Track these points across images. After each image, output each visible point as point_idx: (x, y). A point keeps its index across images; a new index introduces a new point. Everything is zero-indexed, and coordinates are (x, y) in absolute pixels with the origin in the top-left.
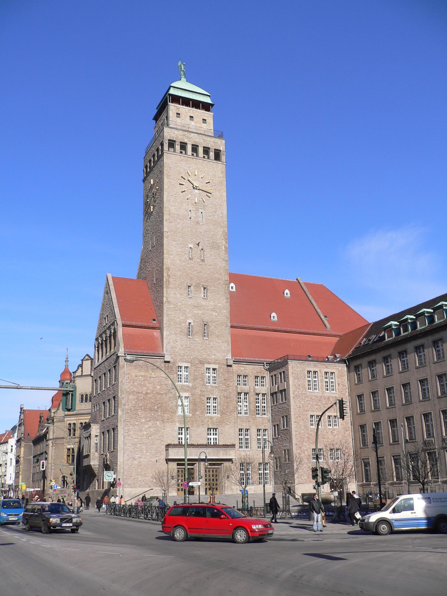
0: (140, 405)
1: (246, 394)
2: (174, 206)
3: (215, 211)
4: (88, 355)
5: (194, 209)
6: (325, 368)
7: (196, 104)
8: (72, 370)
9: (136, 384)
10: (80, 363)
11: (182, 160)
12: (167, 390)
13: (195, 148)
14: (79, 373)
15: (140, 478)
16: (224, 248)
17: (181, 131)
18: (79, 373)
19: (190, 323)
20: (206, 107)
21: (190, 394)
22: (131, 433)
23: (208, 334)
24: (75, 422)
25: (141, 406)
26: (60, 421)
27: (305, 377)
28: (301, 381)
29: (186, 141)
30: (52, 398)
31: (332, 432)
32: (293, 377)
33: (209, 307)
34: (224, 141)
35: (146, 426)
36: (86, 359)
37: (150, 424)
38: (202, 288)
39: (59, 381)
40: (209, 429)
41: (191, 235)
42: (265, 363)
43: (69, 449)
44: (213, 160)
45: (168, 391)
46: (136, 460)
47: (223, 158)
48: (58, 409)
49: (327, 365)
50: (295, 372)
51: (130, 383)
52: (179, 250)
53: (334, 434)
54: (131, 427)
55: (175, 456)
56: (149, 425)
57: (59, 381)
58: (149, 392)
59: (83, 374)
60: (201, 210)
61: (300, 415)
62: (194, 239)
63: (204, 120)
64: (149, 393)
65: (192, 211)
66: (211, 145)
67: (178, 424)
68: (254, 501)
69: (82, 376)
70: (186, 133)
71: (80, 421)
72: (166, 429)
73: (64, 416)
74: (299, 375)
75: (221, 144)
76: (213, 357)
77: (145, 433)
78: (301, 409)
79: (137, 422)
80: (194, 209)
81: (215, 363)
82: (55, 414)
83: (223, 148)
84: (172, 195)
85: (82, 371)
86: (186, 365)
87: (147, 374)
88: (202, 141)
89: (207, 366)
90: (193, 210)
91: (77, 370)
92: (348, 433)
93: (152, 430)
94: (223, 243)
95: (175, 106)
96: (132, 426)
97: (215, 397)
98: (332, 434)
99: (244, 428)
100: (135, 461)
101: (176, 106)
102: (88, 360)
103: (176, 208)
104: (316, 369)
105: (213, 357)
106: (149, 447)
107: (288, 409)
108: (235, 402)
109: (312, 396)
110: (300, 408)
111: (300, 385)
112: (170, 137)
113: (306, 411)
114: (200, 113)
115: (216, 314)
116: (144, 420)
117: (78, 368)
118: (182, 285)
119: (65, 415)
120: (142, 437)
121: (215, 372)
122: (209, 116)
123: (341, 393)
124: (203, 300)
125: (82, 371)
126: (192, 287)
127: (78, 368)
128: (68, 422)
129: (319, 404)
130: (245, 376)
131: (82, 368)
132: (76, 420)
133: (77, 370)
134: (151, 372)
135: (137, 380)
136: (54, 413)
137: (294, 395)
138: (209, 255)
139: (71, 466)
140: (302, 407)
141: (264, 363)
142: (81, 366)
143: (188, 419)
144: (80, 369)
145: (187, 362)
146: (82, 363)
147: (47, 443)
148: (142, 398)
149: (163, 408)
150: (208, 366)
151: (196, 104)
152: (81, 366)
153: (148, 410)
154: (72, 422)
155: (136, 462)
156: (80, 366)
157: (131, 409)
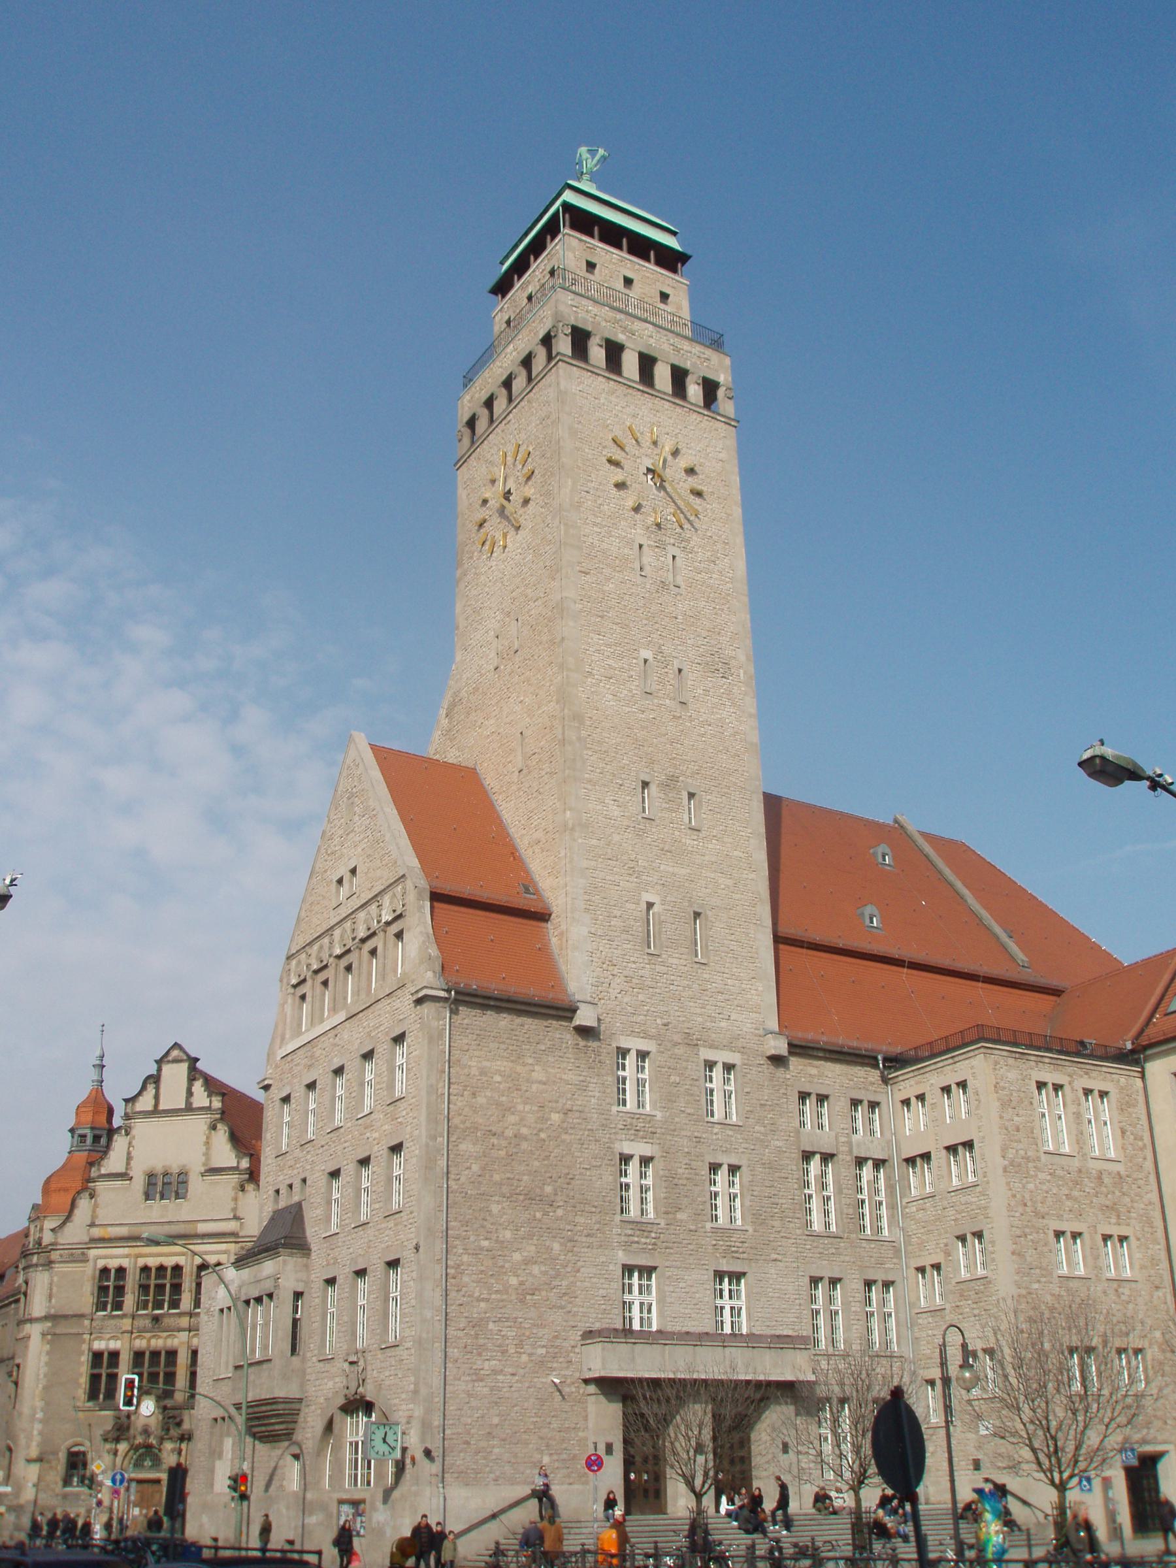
0: (497, 1177)
1: (733, 1169)
2: (595, 524)
3: (713, 558)
4: (176, 1046)
5: (652, 543)
6: (1082, 1077)
7: (640, 247)
8: (115, 1096)
9: (481, 1100)
10: (153, 1070)
11: (613, 392)
12: (585, 1130)
13: (647, 363)
14: (146, 1103)
15: (496, 1450)
16: (742, 675)
17: (607, 308)
18: (146, 1103)
19: (650, 905)
20: (670, 260)
21: (656, 1147)
22: (466, 1279)
23: (707, 946)
24: (125, 1263)
25: (501, 1184)
26: (73, 1260)
27: (1031, 1103)
28: (1021, 1112)
29: (621, 338)
30: (48, 1182)
31: (1117, 1291)
32: (999, 1099)
33: (707, 858)
34: (727, 361)
35: (517, 1256)
36: (170, 1058)
37: (530, 1249)
38: (685, 795)
39: (72, 1131)
40: (719, 1275)
41: (645, 622)
42: (880, 1057)
43: (97, 1356)
44: (700, 407)
45: (586, 1133)
46: (482, 1380)
47: (725, 405)
48: (68, 1218)
49: (1088, 1067)
50: (1002, 1084)
51: (462, 1096)
52: (611, 662)
53: (1123, 1298)
54: (465, 1258)
55: (621, 1369)
56: (526, 1254)
57: (72, 1131)
58: (524, 1131)
59: (161, 1107)
60: (672, 551)
61: (1027, 1230)
62: (655, 636)
63: (664, 297)
64: (525, 1138)
65: (645, 548)
66: (693, 365)
67: (620, 1253)
68: (813, 1539)
69: (156, 1112)
70: (620, 316)
71: (141, 1262)
72: (582, 1270)
73: (86, 1243)
74: (1015, 1094)
75: (720, 369)
76: (723, 1024)
77: (514, 1281)
78: (1028, 1209)
79: (486, 1239)
80: (652, 543)
81: (729, 1047)
82: (59, 1234)
83: (725, 379)
84: (586, 489)
85: (157, 1097)
86: (644, 1045)
87: (519, 1069)
88: (666, 347)
89: (707, 1054)
90: (649, 546)
91: (140, 1094)
92: (1161, 1294)
93: (536, 1270)
94: (740, 655)
95: (581, 240)
96: (469, 1254)
97: (734, 1161)
98: (1119, 1297)
99: (827, 1274)
100: (481, 1384)
101: (586, 242)
102: (181, 1061)
103: (599, 530)
104: (1059, 1078)
105: (723, 1024)
106: (527, 1333)
107: (985, 1208)
108: (796, 1186)
109: (1054, 1167)
110: (1025, 1205)
111: (1021, 1127)
112: (576, 319)
113: (1043, 1218)
114: (648, 273)
115: (730, 882)
116: (508, 1235)
117: (144, 1088)
118: (623, 776)
119: (93, 1240)
120: (505, 1297)
121: (732, 1077)
122: (676, 284)
123: (1131, 1161)
124: (689, 832)
125: (157, 1097)
126: (653, 787)
127: (144, 1088)
128: (101, 1263)
129: (1076, 1193)
130: (822, 1099)
131: (157, 1089)
132: (127, 1256)
133: (140, 1094)
134: (530, 1061)
135: (487, 1088)
136: (53, 1230)
137: (1006, 1163)
138: (701, 692)
139: (103, 1413)
140: (1029, 1204)
141: (876, 1058)
142: (154, 1079)
143: (653, 1235)
144: (151, 1090)
145: (646, 1036)
146: (159, 1070)
147: (19, 1332)
148: (502, 1153)
149: (572, 1194)
150: (711, 1055)
151: (640, 247)
152: (154, 1079)
153: (521, 1198)
154: (113, 1264)
155: (482, 1389)
156: (152, 1080)
157: (466, 1193)
